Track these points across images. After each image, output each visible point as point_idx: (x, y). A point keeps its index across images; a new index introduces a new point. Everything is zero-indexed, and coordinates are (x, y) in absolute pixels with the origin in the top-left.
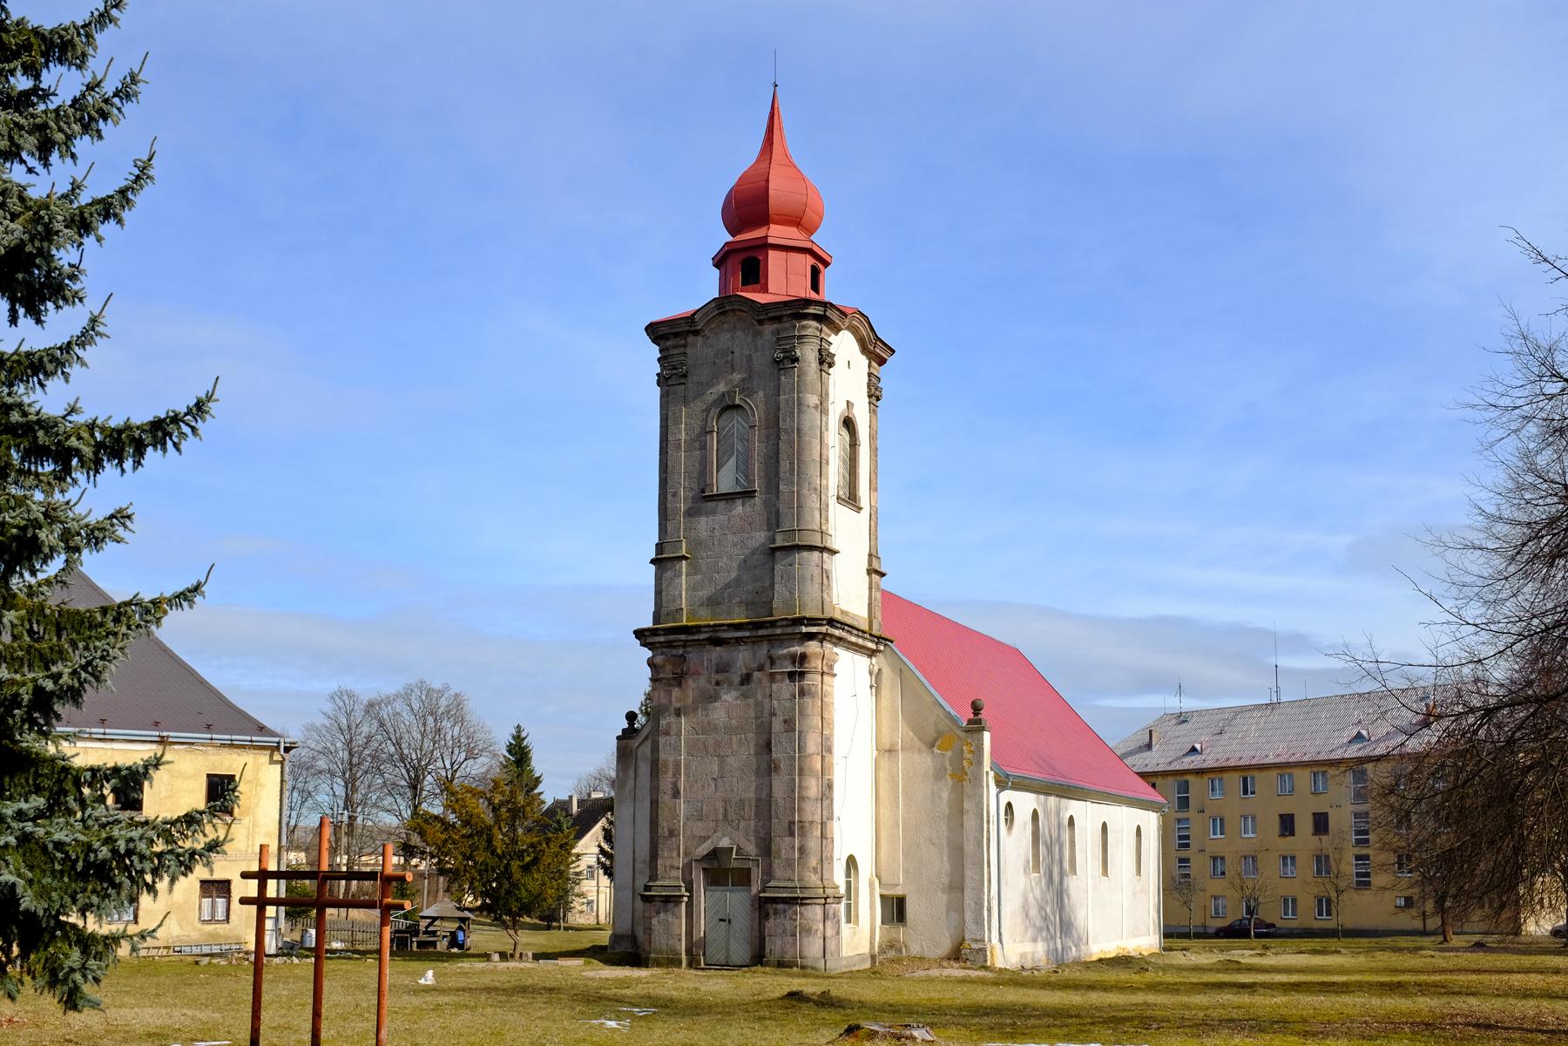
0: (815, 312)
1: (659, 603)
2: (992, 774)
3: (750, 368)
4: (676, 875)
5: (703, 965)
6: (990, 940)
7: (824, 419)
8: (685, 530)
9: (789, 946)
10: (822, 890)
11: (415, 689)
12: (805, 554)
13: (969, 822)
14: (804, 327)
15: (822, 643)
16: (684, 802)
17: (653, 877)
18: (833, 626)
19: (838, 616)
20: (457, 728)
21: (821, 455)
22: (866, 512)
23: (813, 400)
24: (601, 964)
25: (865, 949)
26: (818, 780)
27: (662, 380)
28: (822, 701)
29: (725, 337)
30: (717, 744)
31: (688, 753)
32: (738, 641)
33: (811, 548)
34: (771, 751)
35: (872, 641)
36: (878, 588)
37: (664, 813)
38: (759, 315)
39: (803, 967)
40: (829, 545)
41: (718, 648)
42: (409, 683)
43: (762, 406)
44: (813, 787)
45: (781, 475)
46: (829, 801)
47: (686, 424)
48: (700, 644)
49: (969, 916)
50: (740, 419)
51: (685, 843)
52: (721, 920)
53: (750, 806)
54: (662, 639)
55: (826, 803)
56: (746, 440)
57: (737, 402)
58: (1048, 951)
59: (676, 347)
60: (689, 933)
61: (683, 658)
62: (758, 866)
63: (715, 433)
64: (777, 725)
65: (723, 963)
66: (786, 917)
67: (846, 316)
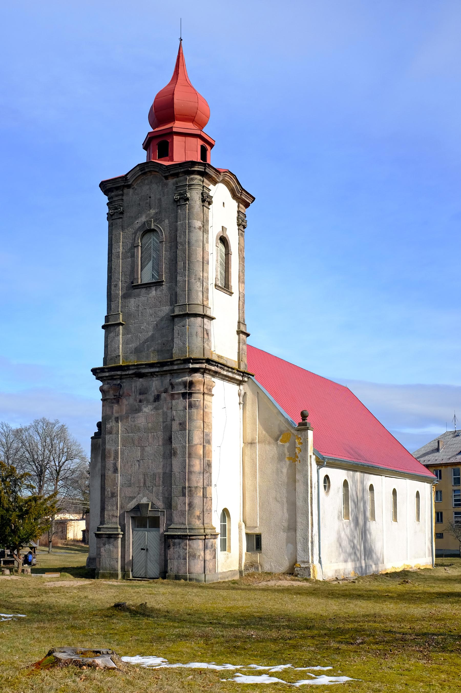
0: (199, 169)
1: (106, 353)
2: (314, 457)
3: (160, 206)
4: (115, 521)
5: (131, 577)
6: (313, 562)
7: (205, 236)
8: (122, 307)
9: (182, 566)
10: (203, 530)
11: (40, 423)
12: (192, 319)
13: (300, 487)
14: (192, 179)
15: (203, 375)
16: (120, 475)
17: (102, 522)
18: (209, 364)
19: (215, 358)
20: (62, 444)
21: (203, 258)
22: (236, 295)
23: (198, 224)
24: (72, 577)
25: (236, 568)
26: (201, 460)
27: (110, 217)
28: (203, 411)
29: (146, 188)
30: (140, 439)
31: (123, 445)
32: (152, 374)
33: (196, 315)
34: (171, 442)
35: (240, 375)
36: (244, 343)
37: (108, 483)
38: (165, 173)
39: (191, 579)
40: (208, 313)
41: (141, 379)
42: (37, 419)
43: (167, 229)
44: (197, 466)
45: (178, 270)
46: (208, 474)
47: (123, 243)
48: (130, 377)
49: (299, 547)
50: (154, 238)
51: (121, 501)
52: (142, 549)
53: (159, 478)
54: (107, 374)
55: (206, 475)
56: (157, 250)
57: (153, 227)
58: (355, 568)
59: (117, 196)
60: (123, 557)
61: (119, 386)
62: (164, 515)
63: (140, 247)
64: (175, 426)
65: (143, 576)
66: (180, 547)
67: (220, 173)
